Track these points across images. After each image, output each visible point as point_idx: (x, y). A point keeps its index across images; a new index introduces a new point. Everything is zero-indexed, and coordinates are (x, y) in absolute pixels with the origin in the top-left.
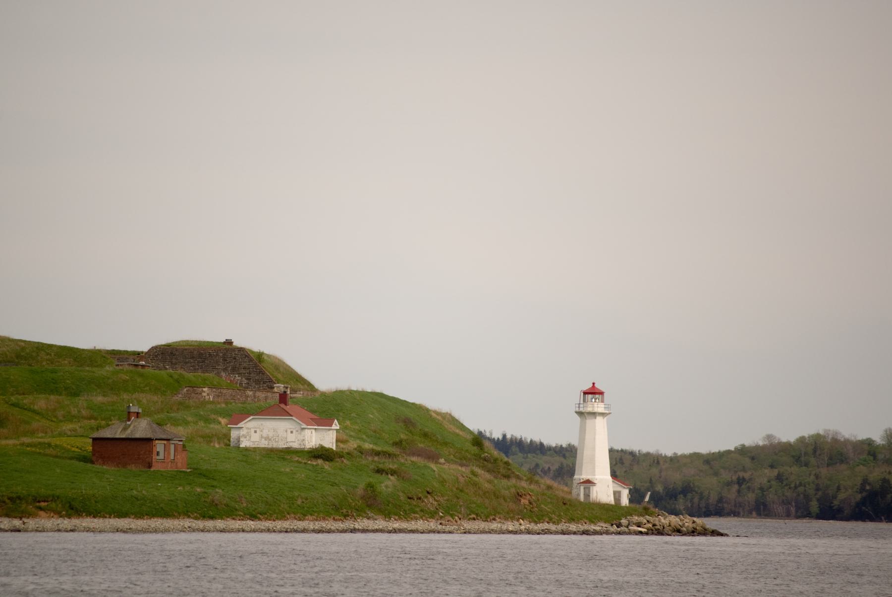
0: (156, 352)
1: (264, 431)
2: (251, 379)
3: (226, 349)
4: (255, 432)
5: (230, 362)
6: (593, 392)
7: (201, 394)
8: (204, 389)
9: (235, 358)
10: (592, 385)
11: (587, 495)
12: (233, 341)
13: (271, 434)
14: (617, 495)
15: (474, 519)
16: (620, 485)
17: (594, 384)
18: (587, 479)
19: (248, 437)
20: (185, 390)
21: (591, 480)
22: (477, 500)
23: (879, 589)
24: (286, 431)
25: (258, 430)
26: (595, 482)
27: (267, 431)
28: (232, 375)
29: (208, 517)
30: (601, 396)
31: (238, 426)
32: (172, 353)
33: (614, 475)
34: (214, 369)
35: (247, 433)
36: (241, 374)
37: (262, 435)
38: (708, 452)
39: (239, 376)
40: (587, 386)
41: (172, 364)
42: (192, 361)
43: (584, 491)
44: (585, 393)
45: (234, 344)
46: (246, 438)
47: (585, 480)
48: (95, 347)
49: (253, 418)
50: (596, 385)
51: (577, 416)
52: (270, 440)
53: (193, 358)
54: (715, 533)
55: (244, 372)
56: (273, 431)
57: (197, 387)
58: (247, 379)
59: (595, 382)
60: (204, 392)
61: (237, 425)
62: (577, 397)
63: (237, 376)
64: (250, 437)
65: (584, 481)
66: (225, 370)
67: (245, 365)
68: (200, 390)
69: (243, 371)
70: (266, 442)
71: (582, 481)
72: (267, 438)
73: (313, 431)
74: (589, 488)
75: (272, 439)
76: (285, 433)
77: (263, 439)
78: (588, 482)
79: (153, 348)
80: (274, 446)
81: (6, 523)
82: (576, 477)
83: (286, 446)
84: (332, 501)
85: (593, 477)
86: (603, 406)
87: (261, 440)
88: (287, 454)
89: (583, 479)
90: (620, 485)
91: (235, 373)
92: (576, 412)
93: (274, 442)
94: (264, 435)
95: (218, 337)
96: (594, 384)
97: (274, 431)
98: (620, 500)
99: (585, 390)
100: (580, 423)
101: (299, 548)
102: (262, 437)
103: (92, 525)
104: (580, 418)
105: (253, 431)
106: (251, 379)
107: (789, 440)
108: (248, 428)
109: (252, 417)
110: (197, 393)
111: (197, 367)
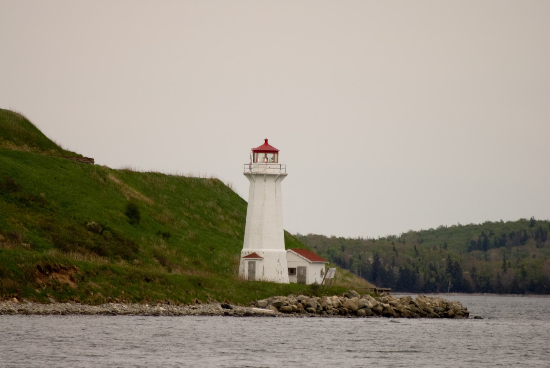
10: (264, 142)
11: (252, 271)
14: (252, 266)
16: (305, 259)
17: (266, 141)
18: (253, 252)
21: (257, 253)
22: (208, 306)
26: (262, 255)
30: (276, 155)
44: (257, 151)
47: (250, 253)
48: (379, 236)
50: (269, 142)
51: (245, 178)
59: (268, 139)
62: (248, 155)
65: (250, 255)
71: (247, 254)
74: (254, 263)
78: (254, 255)
84: (158, 352)
85: (260, 250)
88: (183, 304)
89: (249, 252)
90: (302, 258)
92: (245, 174)
96: (266, 141)
98: (305, 277)
100: (250, 187)
104: (250, 181)
107: (549, 219)
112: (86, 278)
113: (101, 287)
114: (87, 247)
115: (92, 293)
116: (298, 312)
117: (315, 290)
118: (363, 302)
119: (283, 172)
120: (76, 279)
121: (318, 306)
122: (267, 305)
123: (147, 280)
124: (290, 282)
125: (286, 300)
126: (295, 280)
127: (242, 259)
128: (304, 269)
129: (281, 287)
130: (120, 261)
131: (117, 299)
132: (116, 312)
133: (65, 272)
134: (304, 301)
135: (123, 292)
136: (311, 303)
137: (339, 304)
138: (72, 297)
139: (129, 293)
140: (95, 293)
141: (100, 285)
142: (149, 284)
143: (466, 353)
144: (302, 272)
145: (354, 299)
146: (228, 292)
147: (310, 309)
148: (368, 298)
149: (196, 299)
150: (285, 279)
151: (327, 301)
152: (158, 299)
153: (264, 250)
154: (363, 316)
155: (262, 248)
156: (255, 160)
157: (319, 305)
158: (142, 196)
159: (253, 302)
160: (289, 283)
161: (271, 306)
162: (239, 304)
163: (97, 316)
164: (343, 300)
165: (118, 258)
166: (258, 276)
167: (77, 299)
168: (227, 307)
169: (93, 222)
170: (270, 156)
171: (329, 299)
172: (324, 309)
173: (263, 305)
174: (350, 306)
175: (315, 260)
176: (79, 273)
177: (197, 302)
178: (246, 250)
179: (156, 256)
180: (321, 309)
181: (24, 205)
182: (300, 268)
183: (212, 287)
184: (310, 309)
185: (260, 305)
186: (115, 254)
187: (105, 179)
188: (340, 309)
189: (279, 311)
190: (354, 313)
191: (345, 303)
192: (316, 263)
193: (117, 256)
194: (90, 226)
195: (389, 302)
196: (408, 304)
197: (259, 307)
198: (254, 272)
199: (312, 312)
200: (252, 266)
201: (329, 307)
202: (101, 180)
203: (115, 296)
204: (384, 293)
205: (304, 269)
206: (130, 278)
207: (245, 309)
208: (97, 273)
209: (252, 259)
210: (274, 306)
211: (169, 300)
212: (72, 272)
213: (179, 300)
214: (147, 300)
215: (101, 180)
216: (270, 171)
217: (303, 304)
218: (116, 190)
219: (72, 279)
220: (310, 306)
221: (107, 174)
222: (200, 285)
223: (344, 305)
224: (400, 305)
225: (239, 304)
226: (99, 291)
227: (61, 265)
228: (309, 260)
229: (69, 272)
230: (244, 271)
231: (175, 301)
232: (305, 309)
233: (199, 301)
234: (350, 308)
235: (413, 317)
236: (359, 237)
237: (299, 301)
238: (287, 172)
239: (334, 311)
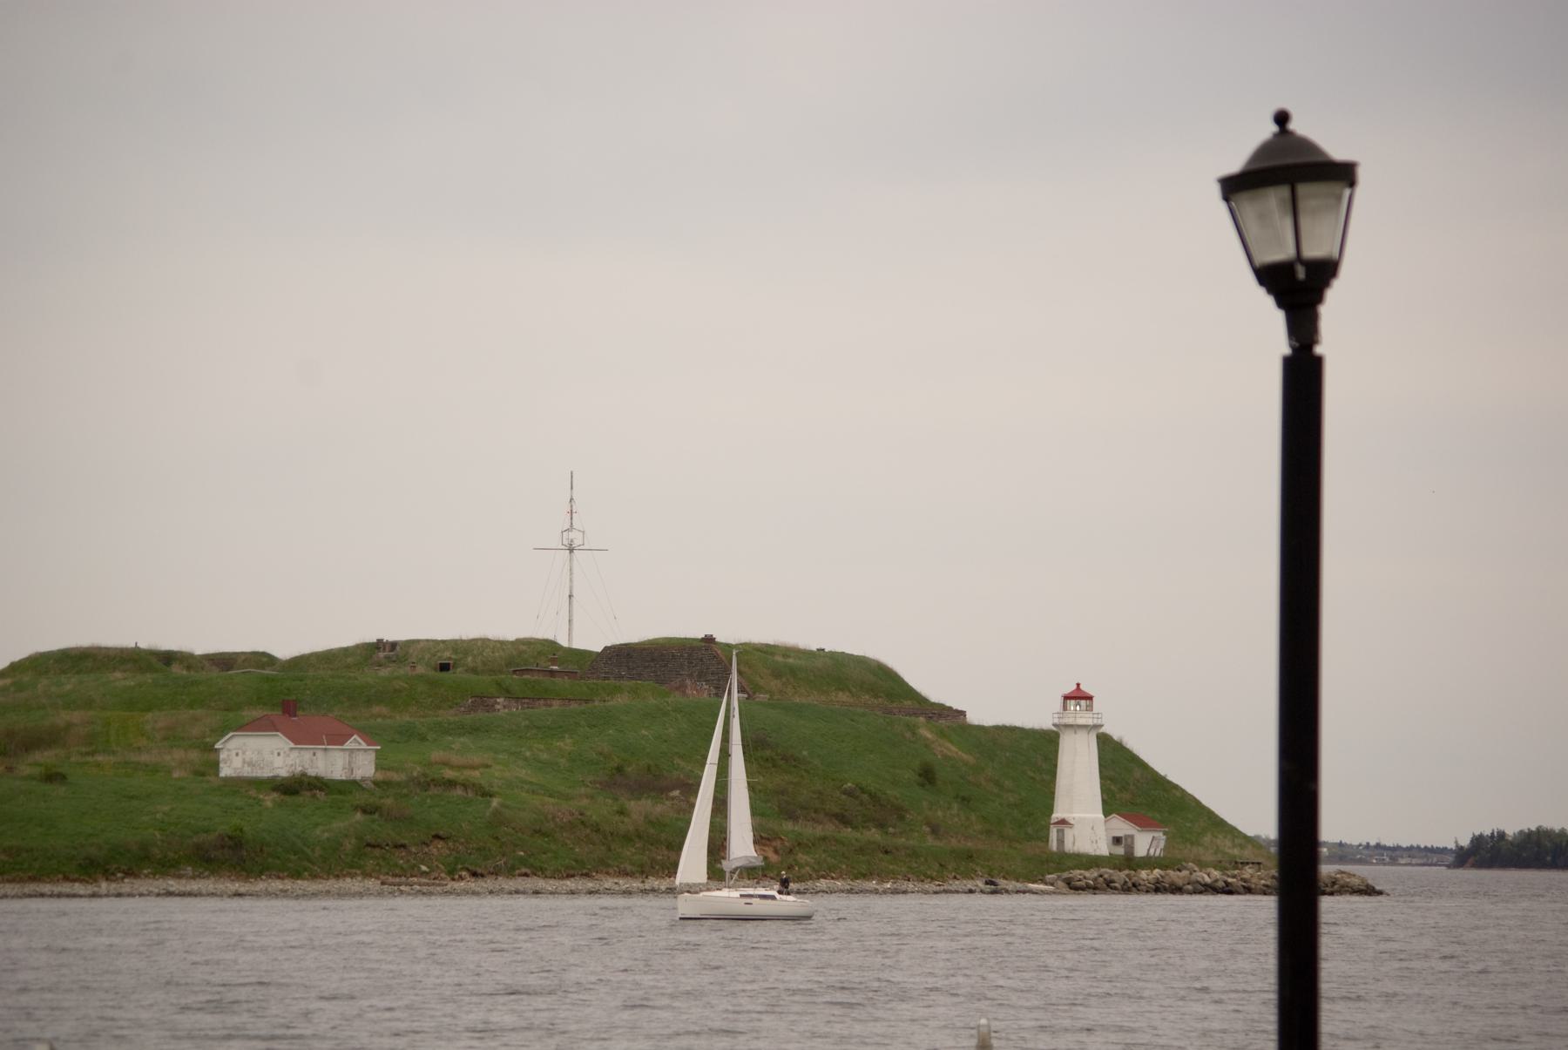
1: (247, 753)
5: (696, 666)
6: (1078, 696)
7: (493, 706)
8: (498, 700)
9: (701, 660)
10: (1075, 687)
11: (1061, 841)
13: (255, 758)
14: (1061, 834)
15: (526, 875)
17: (1078, 685)
20: (470, 701)
23: (1467, 963)
24: (272, 753)
25: (240, 752)
26: (1072, 822)
32: (628, 655)
33: (1109, 808)
40: (1071, 688)
41: (629, 669)
42: (652, 664)
44: (1067, 698)
45: (826, 650)
49: (233, 736)
50: (1081, 687)
52: (254, 766)
53: (653, 660)
54: (1369, 891)
57: (488, 698)
58: (716, 688)
60: (499, 703)
64: (231, 762)
66: (691, 676)
68: (492, 700)
70: (250, 769)
71: (1056, 820)
72: (250, 764)
74: (1063, 831)
77: (246, 765)
78: (1063, 822)
79: (606, 648)
80: (259, 775)
81: (9, 888)
82: (1054, 816)
86: (1091, 715)
94: (247, 760)
95: (698, 633)
96: (1078, 685)
99: (1066, 693)
102: (244, 762)
105: (234, 752)
109: (231, 734)
110: (487, 706)
111: (659, 673)
113: (813, 861)
114: (826, 814)
115: (797, 869)
116: (1095, 888)
117: (1148, 862)
119: (1099, 722)
120: (781, 852)
121: (1126, 882)
123: (886, 852)
124: (1110, 854)
125: (1080, 875)
126: (1120, 851)
128: (1132, 837)
129: (1084, 860)
130: (870, 830)
131: (834, 875)
132: (668, 893)
133: (768, 843)
134: (1106, 876)
135: (844, 867)
136: (1115, 878)
137: (1158, 879)
138: (766, 872)
139: (853, 868)
140: (801, 866)
141: (812, 858)
142: (888, 857)
143: (600, 939)
144: (1129, 840)
146: (1010, 866)
147: (1112, 885)
149: (953, 874)
150: (1103, 849)
151: (1141, 876)
152: (894, 874)
153: (1074, 815)
154: (1190, 893)
155: (1072, 813)
156: (1065, 708)
157: (1127, 880)
158: (960, 753)
159: (1041, 878)
160: (1108, 854)
162: (1021, 880)
165: (867, 827)
166: (1069, 847)
167: (772, 875)
168: (992, 883)
169: (849, 784)
170: (1083, 702)
171: (1144, 874)
172: (1134, 885)
174: (1173, 881)
175: (1144, 827)
176: (787, 844)
177: (955, 878)
178: (1056, 816)
179: (928, 824)
180: (1130, 884)
181: (770, 765)
182: (1127, 837)
183: (988, 860)
184: (1112, 885)
185: (1048, 881)
186: (865, 822)
187: (914, 734)
188: (1158, 885)
189: (1071, 888)
190: (1176, 889)
191: (1167, 877)
193: (867, 824)
194: (846, 789)
197: (1046, 884)
198: (1063, 842)
199: (1115, 888)
200: (1061, 834)
201: (1142, 883)
202: (908, 735)
203: (830, 872)
205: (1132, 837)
206: (861, 851)
207: (1019, 886)
208: (813, 845)
209: (1061, 827)
211: (909, 876)
212: (778, 843)
213: (924, 876)
214: (878, 875)
215: (908, 735)
216: (1081, 721)
217: (1105, 879)
218: (926, 746)
219: (776, 852)
221: (919, 728)
222: (971, 857)
225: (1021, 880)
226: (807, 864)
227: (763, 835)
229: (774, 844)
231: (918, 876)
232: (1108, 886)
233: (958, 876)
234: (1172, 884)
235: (1265, 894)
238: (1103, 723)
239: (1148, 887)
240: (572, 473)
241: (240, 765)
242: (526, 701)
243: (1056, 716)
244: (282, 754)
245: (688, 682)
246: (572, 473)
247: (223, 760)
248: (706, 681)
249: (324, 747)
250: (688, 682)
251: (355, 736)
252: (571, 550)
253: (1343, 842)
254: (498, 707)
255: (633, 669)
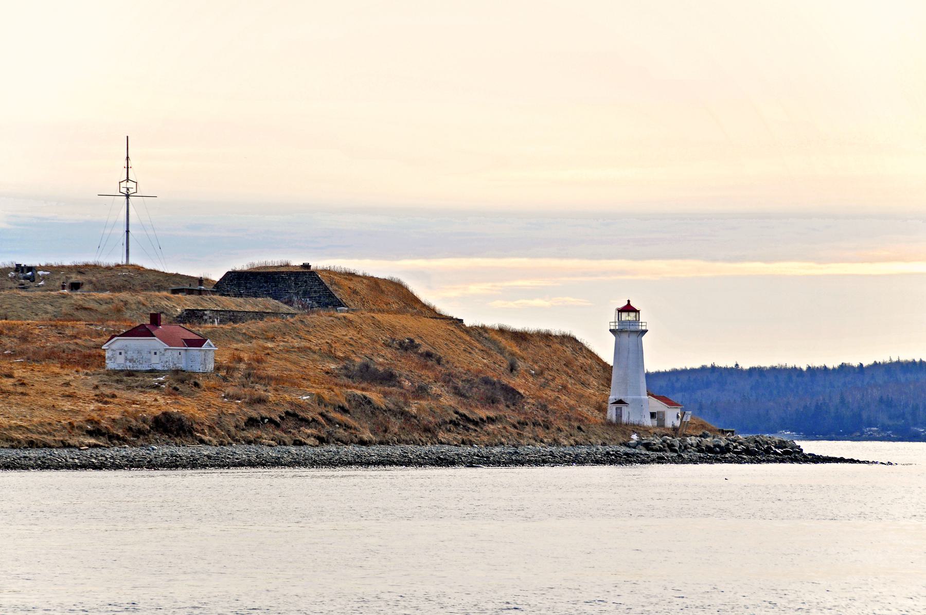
0: (231, 277)
1: (129, 353)
2: (321, 303)
3: (304, 273)
4: (120, 354)
6: (628, 308)
11: (619, 416)
12: (310, 264)
14: (619, 411)
17: (629, 301)
19: (113, 359)
21: (623, 400)
24: (150, 353)
25: (123, 352)
27: (132, 352)
28: (303, 299)
29: (592, 461)
30: (637, 313)
31: (202, 348)
34: (286, 293)
35: (112, 355)
36: (312, 297)
37: (126, 357)
38: (684, 368)
39: (310, 300)
41: (246, 288)
42: (265, 285)
43: (617, 412)
44: (621, 311)
45: (312, 268)
46: (111, 360)
47: (617, 400)
52: (135, 362)
55: (315, 296)
56: (137, 352)
60: (206, 315)
61: (201, 347)
63: (308, 299)
64: (115, 360)
66: (297, 294)
67: (316, 288)
69: (313, 295)
70: (131, 364)
73: (183, 352)
74: (621, 409)
75: (137, 361)
76: (149, 354)
78: (620, 402)
83: (151, 368)
87: (125, 362)
91: (306, 297)
92: (610, 330)
93: (138, 364)
94: (129, 357)
96: (629, 301)
97: (138, 353)
101: (253, 479)
102: (126, 359)
103: (300, 474)
106: (321, 303)
108: (113, 350)
112: (310, 435)
118: (717, 441)
122: (637, 445)
127: (609, 405)
128: (663, 413)
145: (708, 439)
148: (719, 438)
161: (641, 447)
163: (171, 365)
164: (700, 440)
173: (633, 445)
192: (673, 408)
195: (738, 441)
196: (752, 442)
198: (621, 416)
200: (619, 411)
204: (729, 433)
209: (619, 405)
210: (643, 446)
220: (674, 446)
223: (701, 445)
224: (747, 444)
228: (667, 405)
230: (611, 416)
234: (707, 447)
236: (891, 360)
237: (664, 441)
240: (127, 137)
241: (123, 362)
242: (222, 313)
243: (613, 324)
244: (158, 353)
245: (295, 299)
246: (127, 137)
247: (109, 358)
248: (310, 297)
249: (186, 348)
250: (295, 299)
251: (208, 341)
252: (128, 196)
253: (878, 362)
254: (205, 317)
255: (250, 288)
